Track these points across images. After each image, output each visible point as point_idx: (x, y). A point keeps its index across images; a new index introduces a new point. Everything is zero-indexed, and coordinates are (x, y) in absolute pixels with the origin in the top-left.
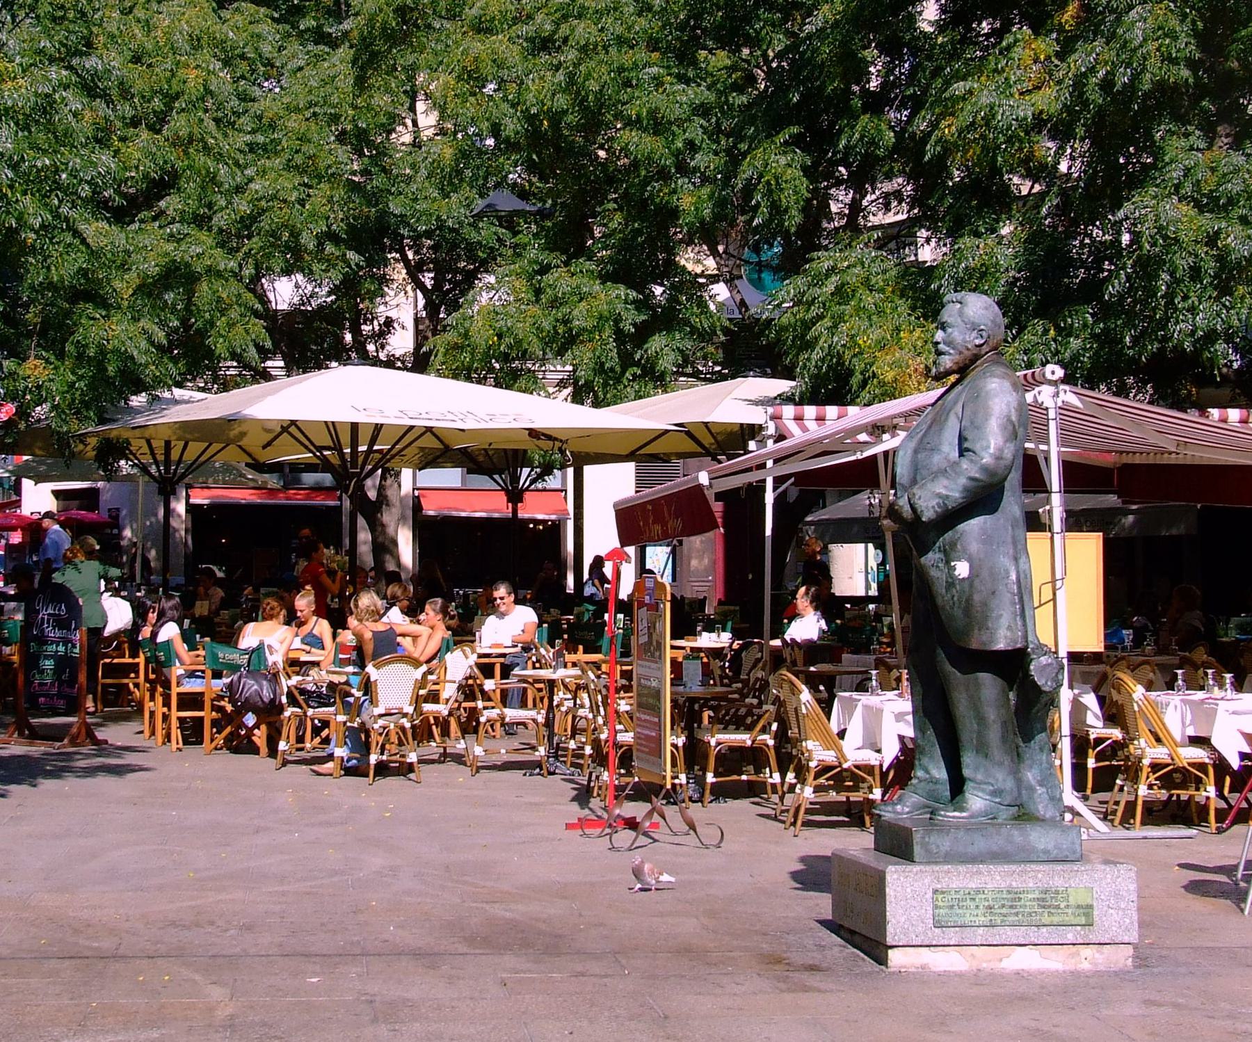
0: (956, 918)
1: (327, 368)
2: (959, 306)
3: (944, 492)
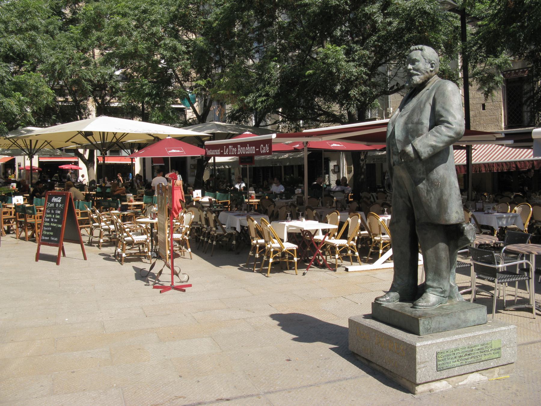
0: (447, 365)
1: (142, 261)
2: (420, 52)
3: (434, 143)
